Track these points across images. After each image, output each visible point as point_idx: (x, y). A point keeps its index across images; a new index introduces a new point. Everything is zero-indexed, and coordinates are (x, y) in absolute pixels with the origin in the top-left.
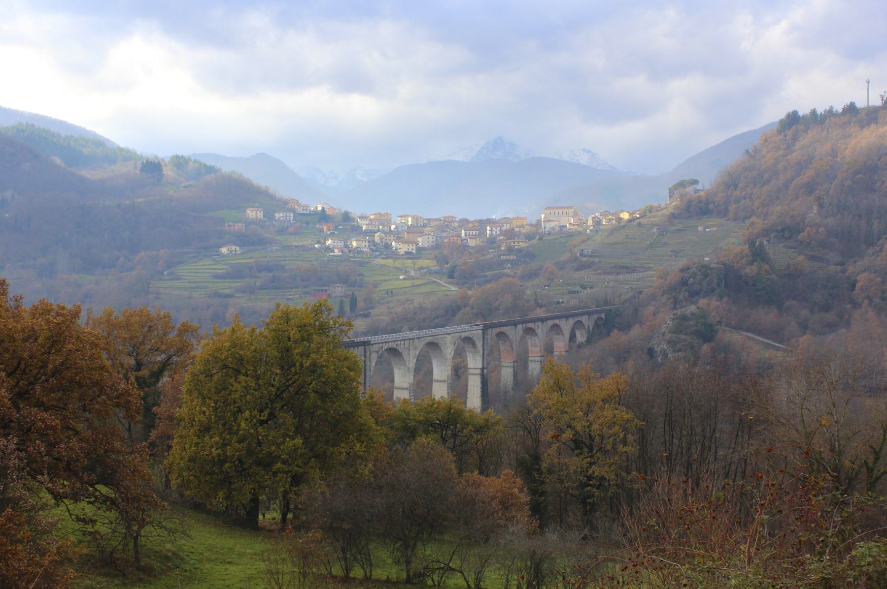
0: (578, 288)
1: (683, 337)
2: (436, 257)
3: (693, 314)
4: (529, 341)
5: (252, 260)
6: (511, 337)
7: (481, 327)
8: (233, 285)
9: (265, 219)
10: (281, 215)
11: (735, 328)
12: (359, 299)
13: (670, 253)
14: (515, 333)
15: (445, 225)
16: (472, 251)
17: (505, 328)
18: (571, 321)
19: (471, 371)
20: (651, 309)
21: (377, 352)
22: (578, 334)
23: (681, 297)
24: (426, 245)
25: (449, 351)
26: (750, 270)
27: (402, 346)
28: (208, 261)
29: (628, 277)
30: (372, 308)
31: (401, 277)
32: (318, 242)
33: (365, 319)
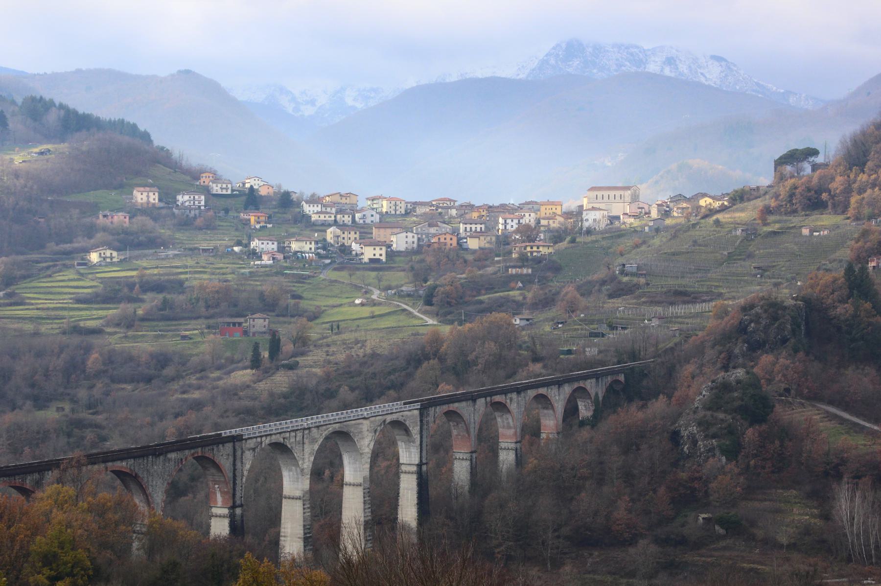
0: (604, 329)
1: (721, 416)
2: (412, 268)
3: (739, 382)
4: (499, 420)
5: (134, 273)
6: (466, 416)
7: (418, 406)
8: (101, 313)
9: (162, 205)
10: (186, 198)
11: (808, 398)
12: (283, 340)
13: (754, 271)
14: (473, 413)
15: (437, 214)
16: (470, 257)
17: (456, 405)
18: (567, 389)
19: (403, 468)
20: (690, 368)
21: (254, 449)
22: (581, 405)
23: (737, 351)
24: (402, 248)
25: (366, 443)
26: (843, 310)
27: (293, 440)
28: (70, 274)
29: (680, 310)
30: (303, 354)
31: (358, 301)
32: (239, 244)
33: (290, 373)
